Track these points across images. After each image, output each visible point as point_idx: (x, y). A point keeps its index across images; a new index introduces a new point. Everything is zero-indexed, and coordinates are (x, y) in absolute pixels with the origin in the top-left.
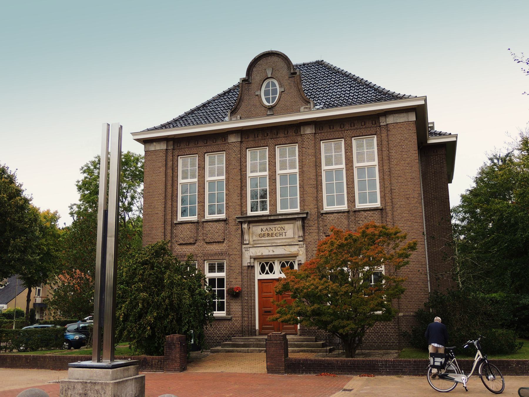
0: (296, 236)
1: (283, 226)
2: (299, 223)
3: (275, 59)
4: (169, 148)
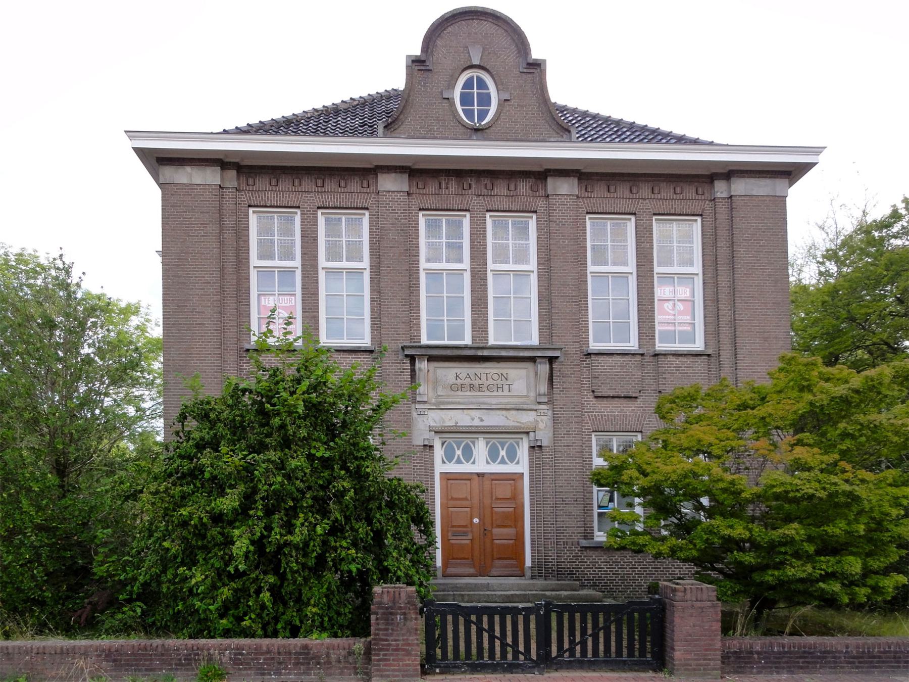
0: (532, 394)
1: (504, 372)
2: (544, 368)
3: (487, 27)
4: (227, 185)
